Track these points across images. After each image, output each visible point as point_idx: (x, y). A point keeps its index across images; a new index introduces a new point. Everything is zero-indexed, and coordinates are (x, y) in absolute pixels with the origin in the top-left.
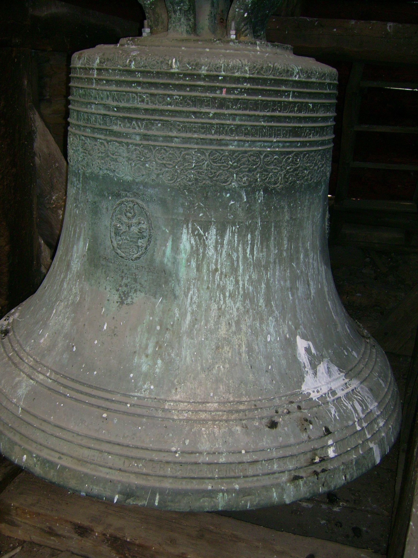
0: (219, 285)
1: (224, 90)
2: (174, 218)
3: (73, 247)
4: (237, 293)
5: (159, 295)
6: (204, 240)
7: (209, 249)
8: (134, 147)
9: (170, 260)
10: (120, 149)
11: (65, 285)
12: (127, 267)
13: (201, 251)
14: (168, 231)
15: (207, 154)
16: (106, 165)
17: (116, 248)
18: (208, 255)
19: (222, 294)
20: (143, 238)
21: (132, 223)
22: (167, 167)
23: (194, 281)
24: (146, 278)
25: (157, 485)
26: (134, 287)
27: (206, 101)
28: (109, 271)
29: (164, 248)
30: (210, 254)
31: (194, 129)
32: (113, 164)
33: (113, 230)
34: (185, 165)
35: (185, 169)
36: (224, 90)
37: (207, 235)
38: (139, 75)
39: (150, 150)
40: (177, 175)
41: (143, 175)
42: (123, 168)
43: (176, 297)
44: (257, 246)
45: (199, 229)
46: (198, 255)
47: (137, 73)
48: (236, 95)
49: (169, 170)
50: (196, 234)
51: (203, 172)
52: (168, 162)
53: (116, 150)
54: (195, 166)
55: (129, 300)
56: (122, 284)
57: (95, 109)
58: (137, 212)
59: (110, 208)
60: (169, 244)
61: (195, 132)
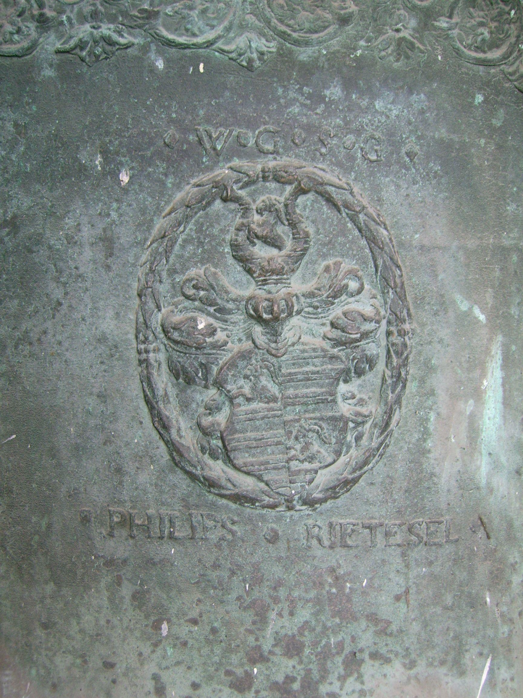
2: (507, 242)
5: (475, 650)
9: (503, 459)
12: (282, 545)
14: (482, 317)
20: (360, 373)
24: (397, 583)
26: (340, 645)
28: (166, 586)
29: (469, 406)
33: (162, 356)
41: (344, 21)
56: (267, 646)
58: (311, 230)
59: (125, 235)
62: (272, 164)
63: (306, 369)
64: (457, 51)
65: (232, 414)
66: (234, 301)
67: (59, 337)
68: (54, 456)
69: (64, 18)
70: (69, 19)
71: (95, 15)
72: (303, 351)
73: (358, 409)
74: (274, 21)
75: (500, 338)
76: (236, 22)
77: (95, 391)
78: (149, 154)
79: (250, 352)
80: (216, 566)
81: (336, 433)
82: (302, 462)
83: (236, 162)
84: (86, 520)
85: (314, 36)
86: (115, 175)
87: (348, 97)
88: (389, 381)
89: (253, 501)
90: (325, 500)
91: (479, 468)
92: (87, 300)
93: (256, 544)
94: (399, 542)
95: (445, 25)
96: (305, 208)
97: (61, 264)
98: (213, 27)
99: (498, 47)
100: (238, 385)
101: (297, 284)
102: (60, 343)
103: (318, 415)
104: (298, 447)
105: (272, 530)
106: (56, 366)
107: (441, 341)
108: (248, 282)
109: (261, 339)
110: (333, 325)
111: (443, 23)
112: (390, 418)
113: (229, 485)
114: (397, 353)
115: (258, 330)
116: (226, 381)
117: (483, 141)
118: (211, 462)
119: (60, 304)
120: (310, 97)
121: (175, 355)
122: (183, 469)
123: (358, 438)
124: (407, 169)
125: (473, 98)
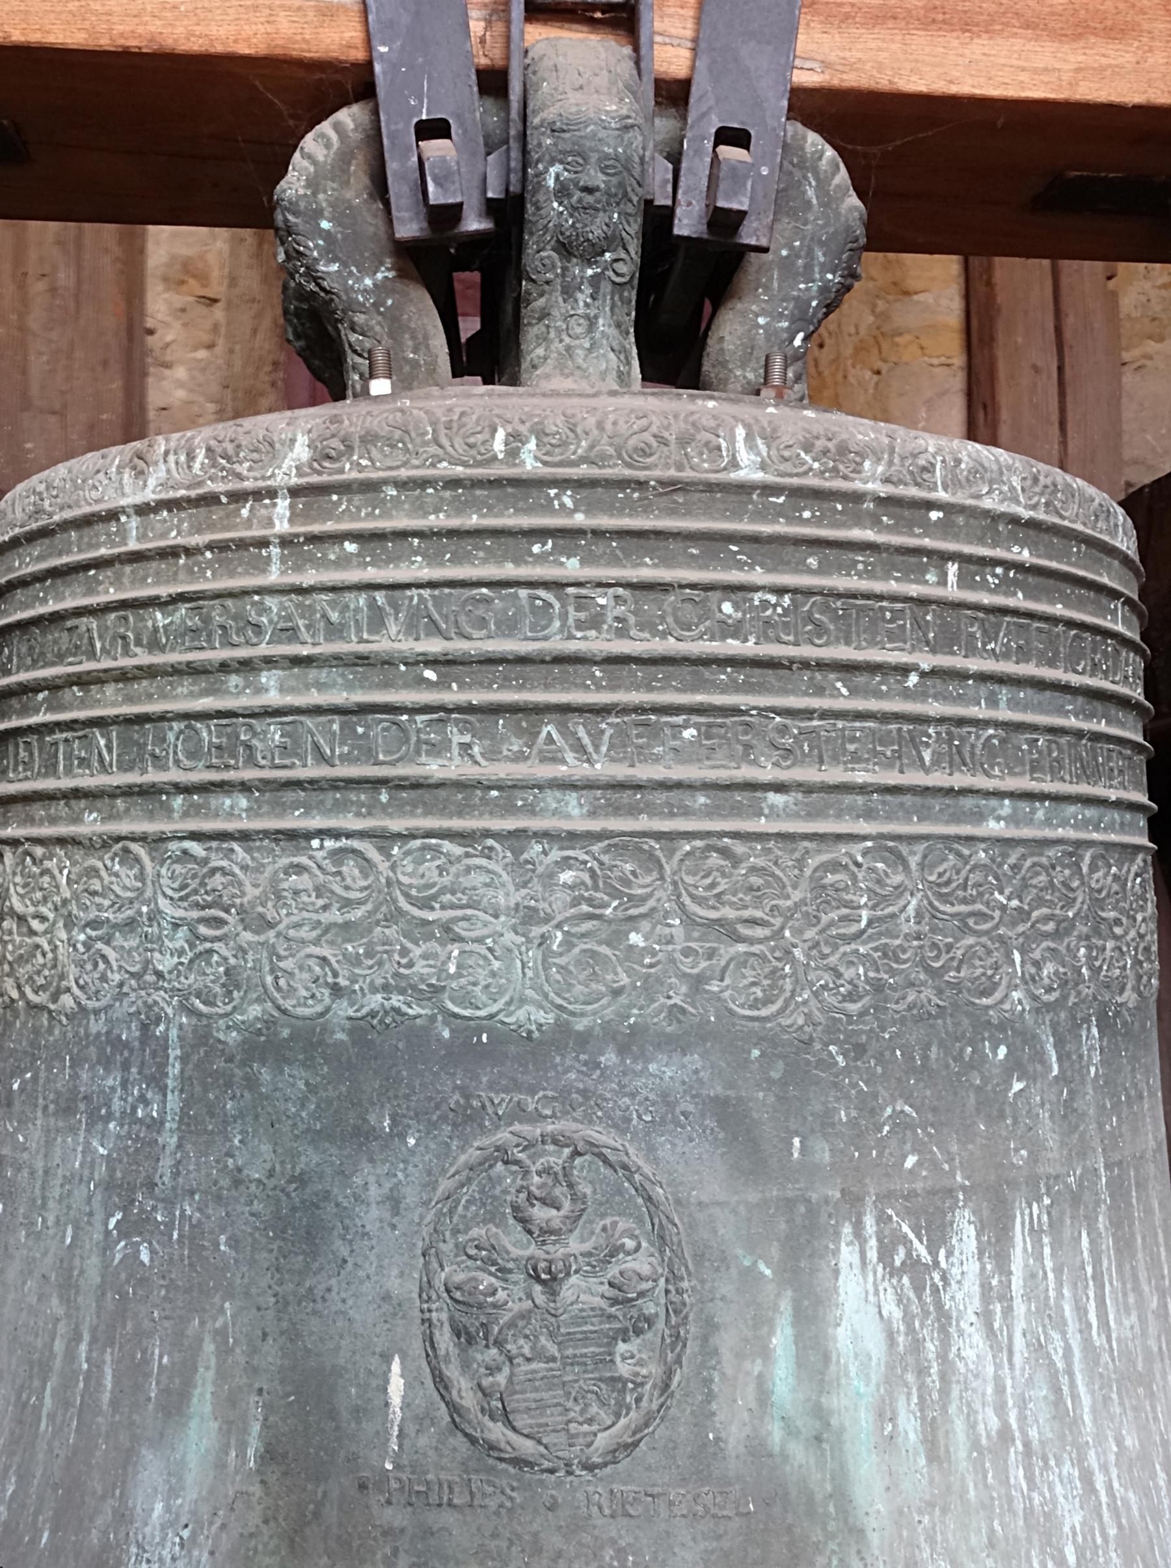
0: (1029, 1512)
1: (953, 569)
2: (790, 1194)
3: (127, 1460)
4: (1099, 1541)
6: (935, 1290)
7: (961, 1333)
8: (556, 854)
10: (468, 870)
13: (931, 1348)
14: (768, 1272)
15: (914, 861)
16: (380, 964)
17: (474, 1413)
18: (960, 1366)
19: (1053, 1558)
20: (638, 1332)
21: (565, 1259)
22: (741, 939)
23: (926, 1520)
27: (888, 615)
29: (757, 1367)
30: (969, 1354)
31: (851, 747)
32: (425, 956)
33: (444, 1316)
34: (825, 919)
35: (827, 943)
36: (953, 569)
37: (943, 1265)
38: (568, 502)
39: (651, 862)
40: (794, 974)
42: (496, 965)
44: (1111, 1283)
45: (911, 1236)
46: (922, 1372)
47: (553, 492)
48: (990, 591)
49: (756, 949)
50: (898, 1263)
51: (904, 951)
52: (746, 914)
53: (446, 880)
54: (870, 923)
57: (282, 690)
58: (588, 1191)
59: (411, 1195)
60: (782, 1340)
61: (856, 758)
62: (550, 1128)
63: (584, 1328)
64: (732, 1013)
65: (512, 1374)
66: (514, 1260)
67: (343, 1295)
68: (334, 1420)
69: (357, 987)
70: (361, 989)
71: (386, 988)
72: (582, 1310)
73: (637, 1369)
74: (552, 995)
75: (789, 1293)
76: (517, 996)
77: (378, 1350)
78: (435, 1118)
79: (530, 1312)
80: (495, 1535)
81: (615, 1395)
82: (581, 1424)
83: (517, 1127)
84: (363, 1487)
85: (589, 1008)
86: (403, 1136)
87: (623, 1061)
88: (668, 1341)
89: (531, 1465)
90: (605, 1465)
91: (770, 1433)
92: (373, 1258)
93: (536, 1510)
94: (685, 1512)
95: (716, 989)
96: (582, 1168)
97: (347, 1222)
98: (495, 1001)
99: (772, 1002)
100: (520, 1346)
101: (574, 1245)
102: (344, 1301)
103: (596, 1375)
104: (578, 1408)
105: (552, 1496)
106: (339, 1324)
107: (723, 1298)
108: (529, 1243)
109: (540, 1299)
110: (611, 1284)
111: (714, 987)
112: (670, 1378)
113: (509, 1449)
114: (675, 1309)
115: (538, 1288)
116: (506, 1341)
117: (761, 1094)
118: (491, 1424)
119: (345, 1261)
120: (586, 1064)
121: (457, 1315)
122: (462, 1431)
123: (638, 1400)
124: (683, 1127)
125: (749, 1053)
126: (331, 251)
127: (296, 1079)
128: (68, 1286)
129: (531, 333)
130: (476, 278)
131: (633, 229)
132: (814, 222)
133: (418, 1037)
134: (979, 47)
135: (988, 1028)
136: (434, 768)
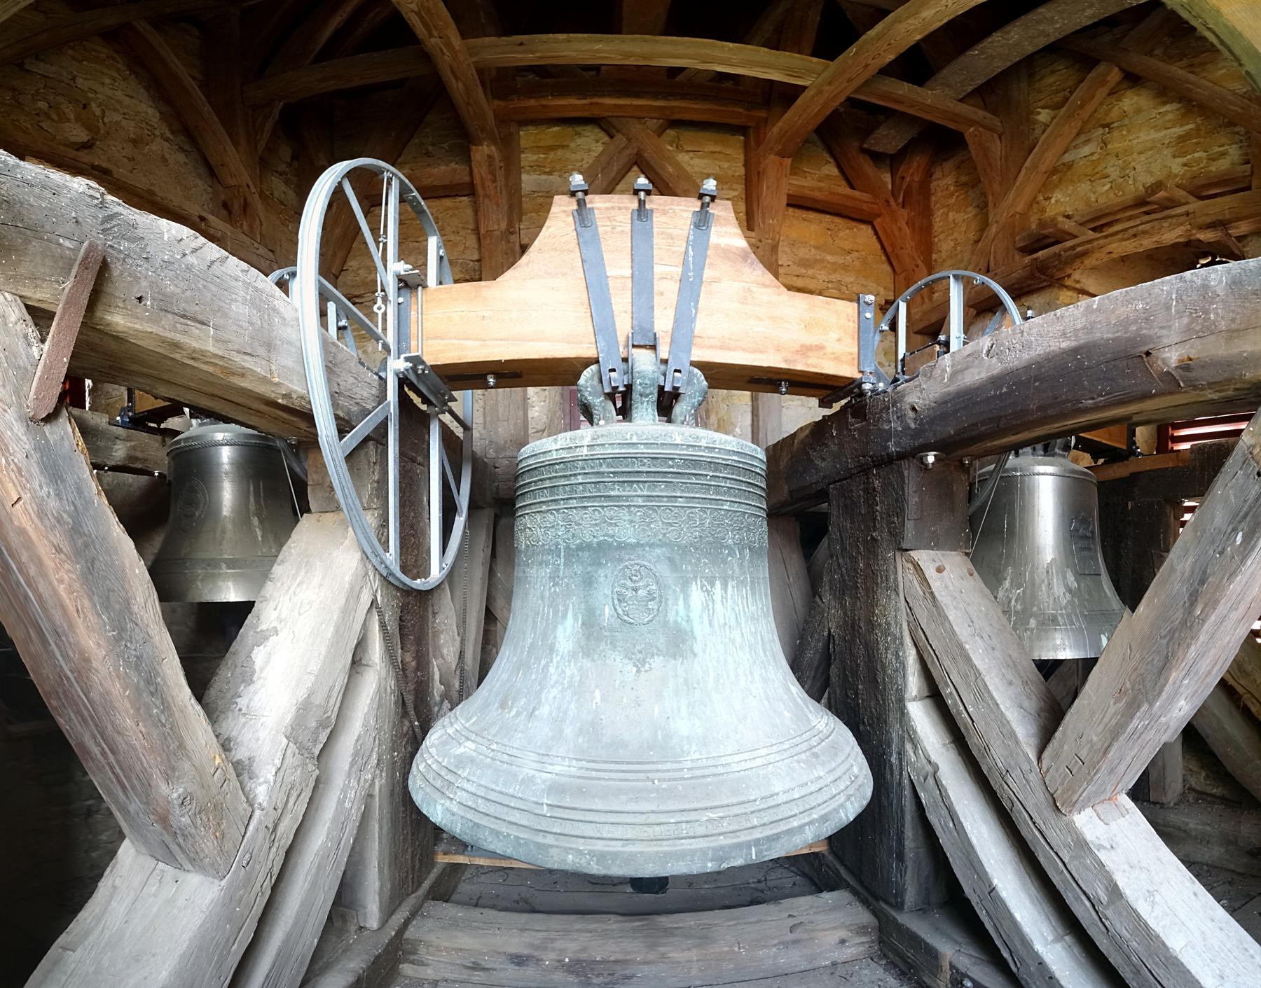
11: (552, 670)
25: (749, 838)
43: (695, 655)
55: (647, 666)
60: (681, 602)
126: (590, 394)
127: (587, 554)
128: (542, 598)
129: (634, 412)
130: (624, 402)
131: (656, 392)
132: (696, 387)
133: (610, 545)
134: (732, 353)
135: (722, 546)
136: (612, 493)
